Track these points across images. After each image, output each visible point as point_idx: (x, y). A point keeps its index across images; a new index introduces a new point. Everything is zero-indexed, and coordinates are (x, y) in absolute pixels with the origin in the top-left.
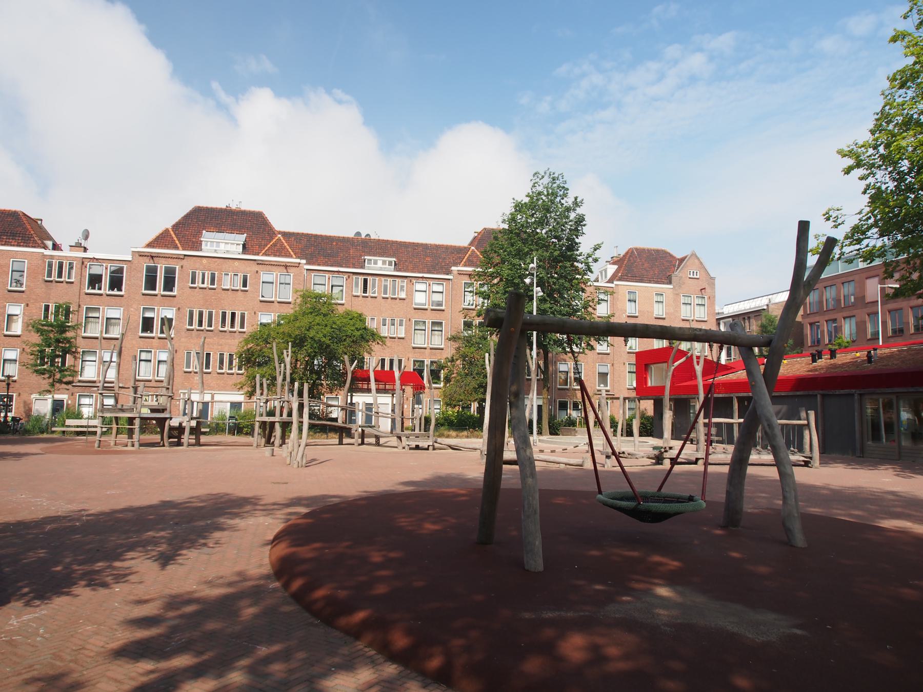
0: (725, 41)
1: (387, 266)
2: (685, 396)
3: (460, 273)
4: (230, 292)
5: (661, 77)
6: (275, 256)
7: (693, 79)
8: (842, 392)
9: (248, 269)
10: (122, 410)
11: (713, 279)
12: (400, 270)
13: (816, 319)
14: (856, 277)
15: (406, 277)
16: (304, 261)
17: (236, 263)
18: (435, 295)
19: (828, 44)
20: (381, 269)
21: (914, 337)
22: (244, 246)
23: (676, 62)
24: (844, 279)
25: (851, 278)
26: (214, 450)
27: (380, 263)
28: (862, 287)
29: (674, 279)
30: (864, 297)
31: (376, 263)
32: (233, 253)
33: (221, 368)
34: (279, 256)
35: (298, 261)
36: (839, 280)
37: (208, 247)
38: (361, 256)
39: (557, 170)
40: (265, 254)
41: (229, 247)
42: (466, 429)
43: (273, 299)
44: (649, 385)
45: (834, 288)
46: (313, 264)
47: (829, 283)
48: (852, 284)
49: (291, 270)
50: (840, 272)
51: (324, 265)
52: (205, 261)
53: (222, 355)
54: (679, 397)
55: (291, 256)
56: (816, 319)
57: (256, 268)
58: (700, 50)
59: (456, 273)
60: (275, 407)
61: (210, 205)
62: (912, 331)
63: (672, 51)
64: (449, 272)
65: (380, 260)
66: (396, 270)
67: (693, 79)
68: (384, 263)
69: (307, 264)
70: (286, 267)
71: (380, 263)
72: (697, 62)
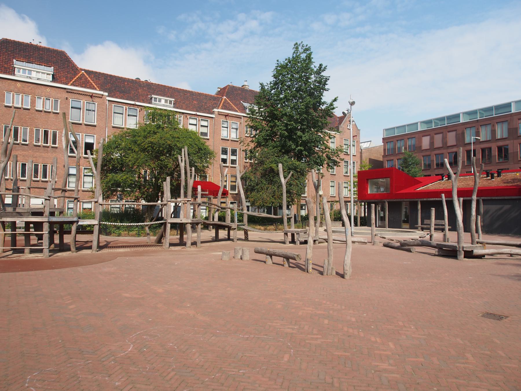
0: (268, 16)
1: (168, 104)
2: (399, 200)
3: (220, 114)
4: (43, 114)
5: (236, 30)
6: (82, 87)
7: (252, 33)
8: (499, 198)
9: (59, 95)
10: (20, 214)
11: (359, 130)
12: (177, 108)
13: (392, 158)
14: (417, 136)
15: (183, 113)
16: (106, 94)
17: (48, 89)
18: (203, 128)
19: (316, 26)
20: (164, 106)
21: (437, 170)
22: (53, 75)
23: (243, 23)
24: (409, 137)
25: (413, 136)
26: (125, 255)
27: (163, 102)
28: (420, 141)
29: (340, 129)
30: (421, 147)
31: (160, 101)
32: (44, 80)
33: (36, 177)
34: (85, 87)
35: (102, 93)
36: (406, 137)
37: (21, 73)
38: (148, 95)
39: (307, 42)
40: (72, 85)
41: (40, 76)
42: (272, 225)
43: (81, 122)
44: (369, 193)
45: (403, 141)
46: (112, 97)
47: (400, 138)
48: (414, 139)
49: (97, 100)
50: (419, 130)
51: (121, 98)
52: (19, 85)
53: (36, 166)
54: (392, 200)
55: (95, 89)
56: (392, 158)
57: (66, 95)
58: (255, 18)
59: (217, 113)
60: (288, 208)
61: (17, 39)
62: (435, 167)
63: (241, 16)
64: (213, 113)
65: (163, 99)
66: (174, 107)
67: (252, 33)
68: (166, 101)
69: (109, 96)
70: (91, 96)
71: (163, 102)
72: (253, 24)
